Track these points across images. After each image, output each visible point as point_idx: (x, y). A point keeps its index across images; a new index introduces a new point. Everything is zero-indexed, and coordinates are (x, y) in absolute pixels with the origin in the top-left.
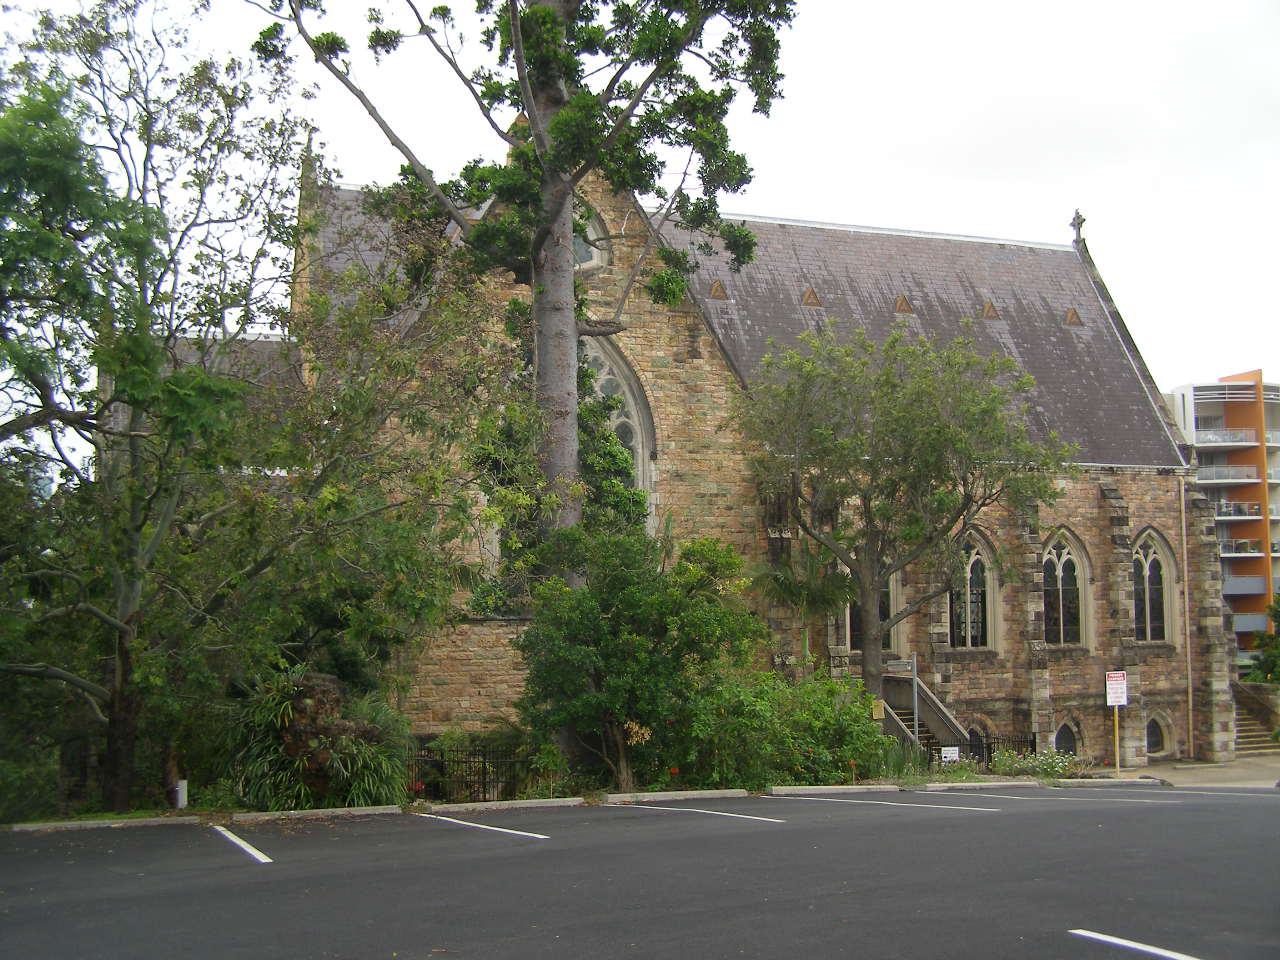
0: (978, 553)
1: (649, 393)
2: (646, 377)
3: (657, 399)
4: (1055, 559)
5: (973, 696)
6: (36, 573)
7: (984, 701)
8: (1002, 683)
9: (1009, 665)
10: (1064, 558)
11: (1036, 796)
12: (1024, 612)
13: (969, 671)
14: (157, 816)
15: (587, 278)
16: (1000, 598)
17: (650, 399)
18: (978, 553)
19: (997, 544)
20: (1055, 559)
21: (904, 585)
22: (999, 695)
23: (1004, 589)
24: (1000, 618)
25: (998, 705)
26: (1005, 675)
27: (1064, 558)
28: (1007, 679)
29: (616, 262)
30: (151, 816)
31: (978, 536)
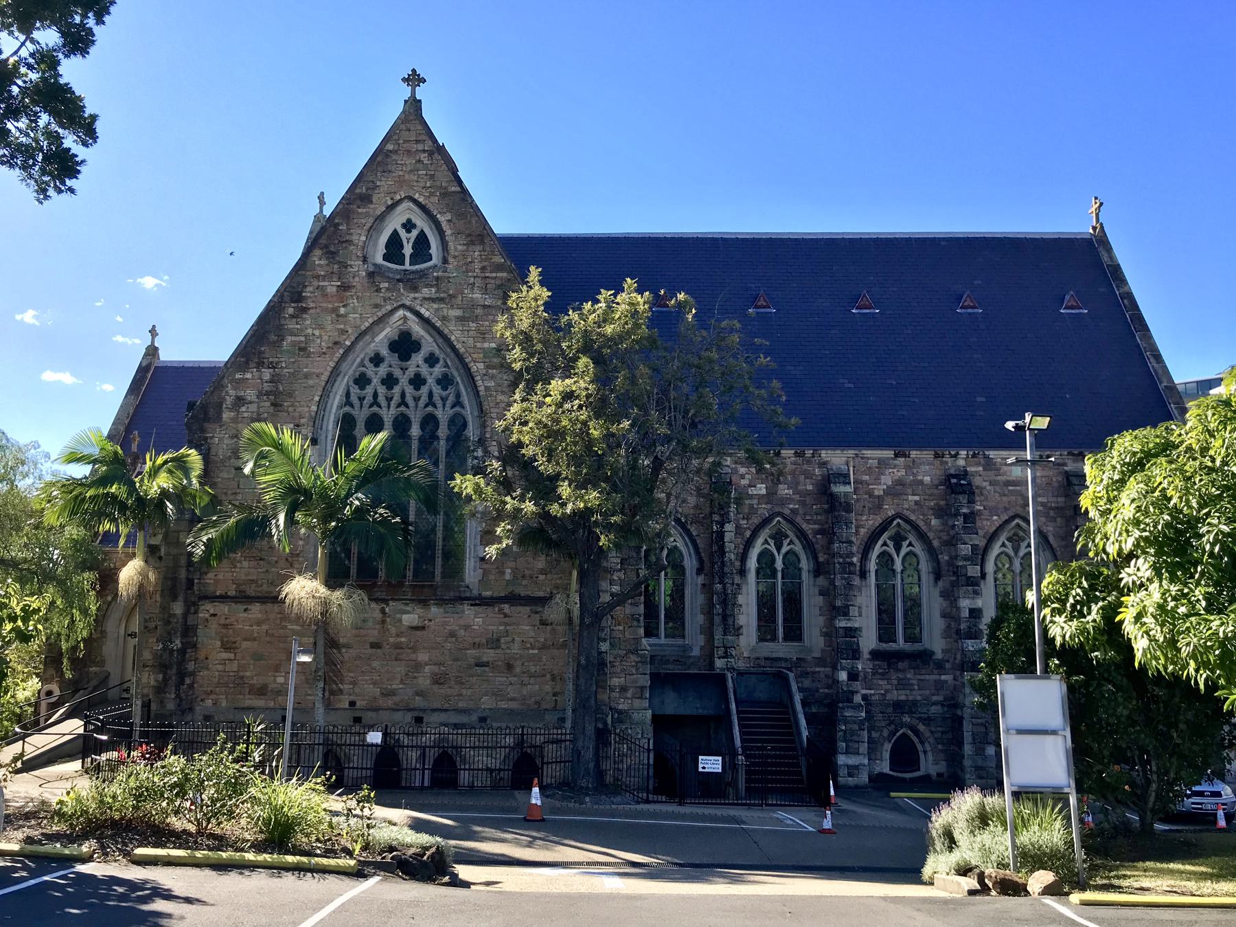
0: (910, 544)
1: (479, 383)
2: (477, 367)
3: (487, 388)
4: (892, 551)
5: (903, 698)
6: (439, 561)
7: (915, 703)
8: (939, 685)
9: (948, 666)
10: (785, 549)
11: (491, 811)
12: (958, 609)
13: (898, 670)
14: (530, 845)
15: (421, 278)
16: (936, 593)
17: (481, 389)
18: (910, 544)
19: (931, 535)
20: (892, 551)
21: (816, 576)
22: (935, 698)
23: (940, 583)
24: (937, 613)
25: (934, 709)
26: (943, 677)
27: (785, 549)
28: (946, 682)
29: (451, 260)
30: (518, 843)
31: (908, 527)
